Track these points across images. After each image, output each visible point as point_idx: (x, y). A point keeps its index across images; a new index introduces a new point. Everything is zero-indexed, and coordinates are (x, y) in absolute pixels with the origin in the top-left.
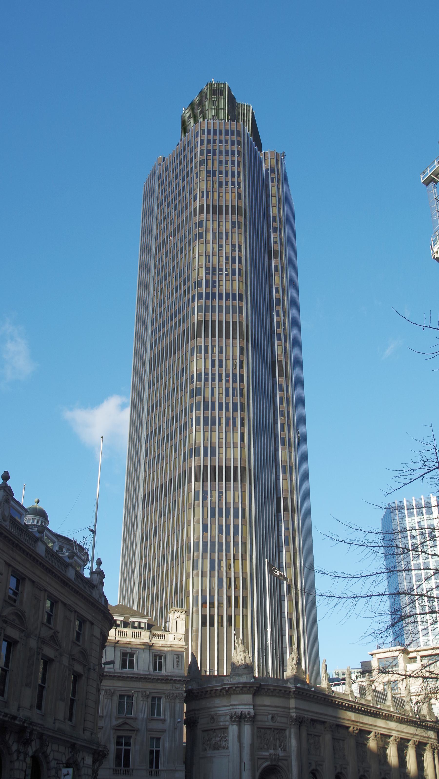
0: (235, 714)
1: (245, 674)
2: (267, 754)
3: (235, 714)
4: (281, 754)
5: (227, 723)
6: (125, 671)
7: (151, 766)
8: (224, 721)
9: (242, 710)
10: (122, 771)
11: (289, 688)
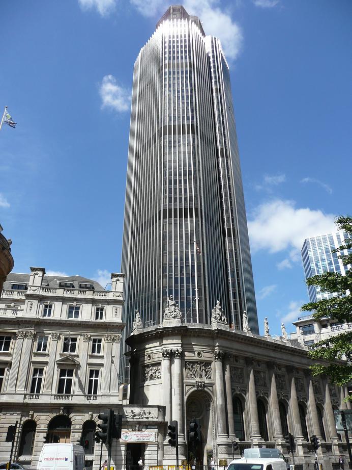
0: (166, 351)
2: (194, 381)
5: (160, 359)
6: (70, 319)
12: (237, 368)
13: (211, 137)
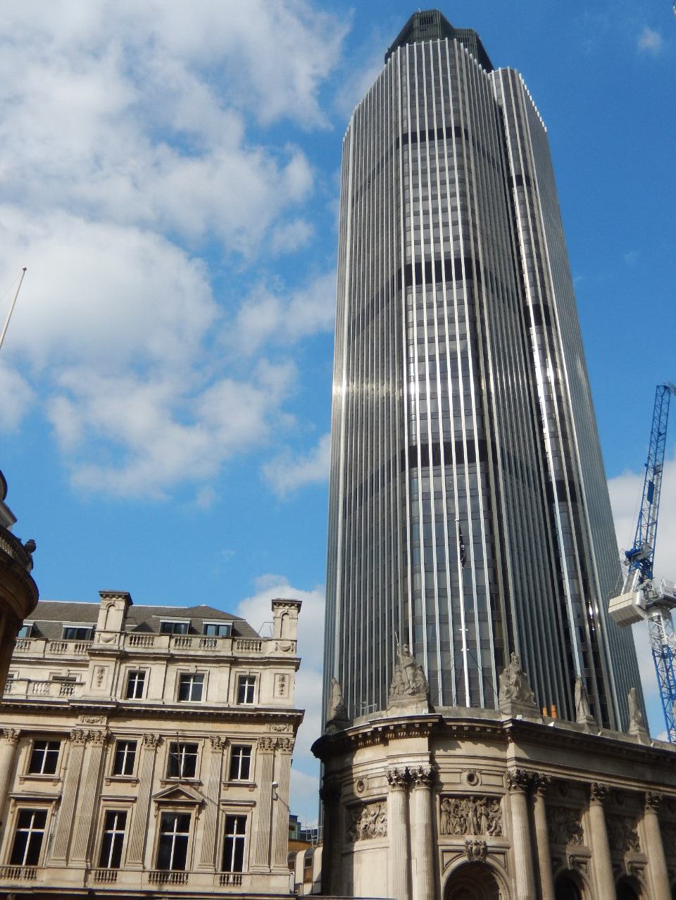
0: (396, 772)
1: (413, 703)
3: (396, 772)
4: (490, 841)
5: (385, 790)
6: (183, 703)
7: (226, 866)
8: (378, 786)
9: (407, 765)
10: (231, 880)
11: (502, 724)
12: (565, 809)
13: (510, 282)
